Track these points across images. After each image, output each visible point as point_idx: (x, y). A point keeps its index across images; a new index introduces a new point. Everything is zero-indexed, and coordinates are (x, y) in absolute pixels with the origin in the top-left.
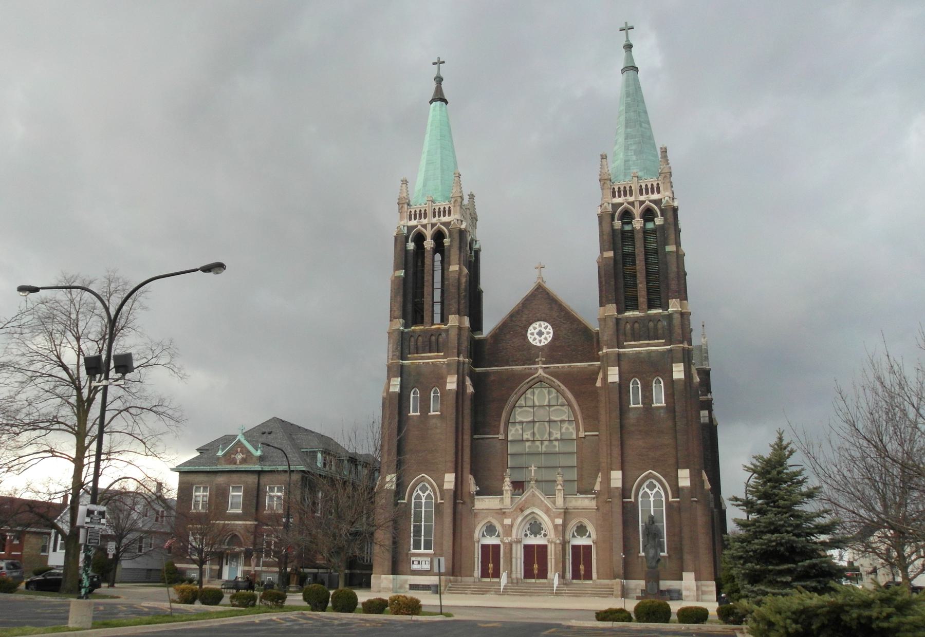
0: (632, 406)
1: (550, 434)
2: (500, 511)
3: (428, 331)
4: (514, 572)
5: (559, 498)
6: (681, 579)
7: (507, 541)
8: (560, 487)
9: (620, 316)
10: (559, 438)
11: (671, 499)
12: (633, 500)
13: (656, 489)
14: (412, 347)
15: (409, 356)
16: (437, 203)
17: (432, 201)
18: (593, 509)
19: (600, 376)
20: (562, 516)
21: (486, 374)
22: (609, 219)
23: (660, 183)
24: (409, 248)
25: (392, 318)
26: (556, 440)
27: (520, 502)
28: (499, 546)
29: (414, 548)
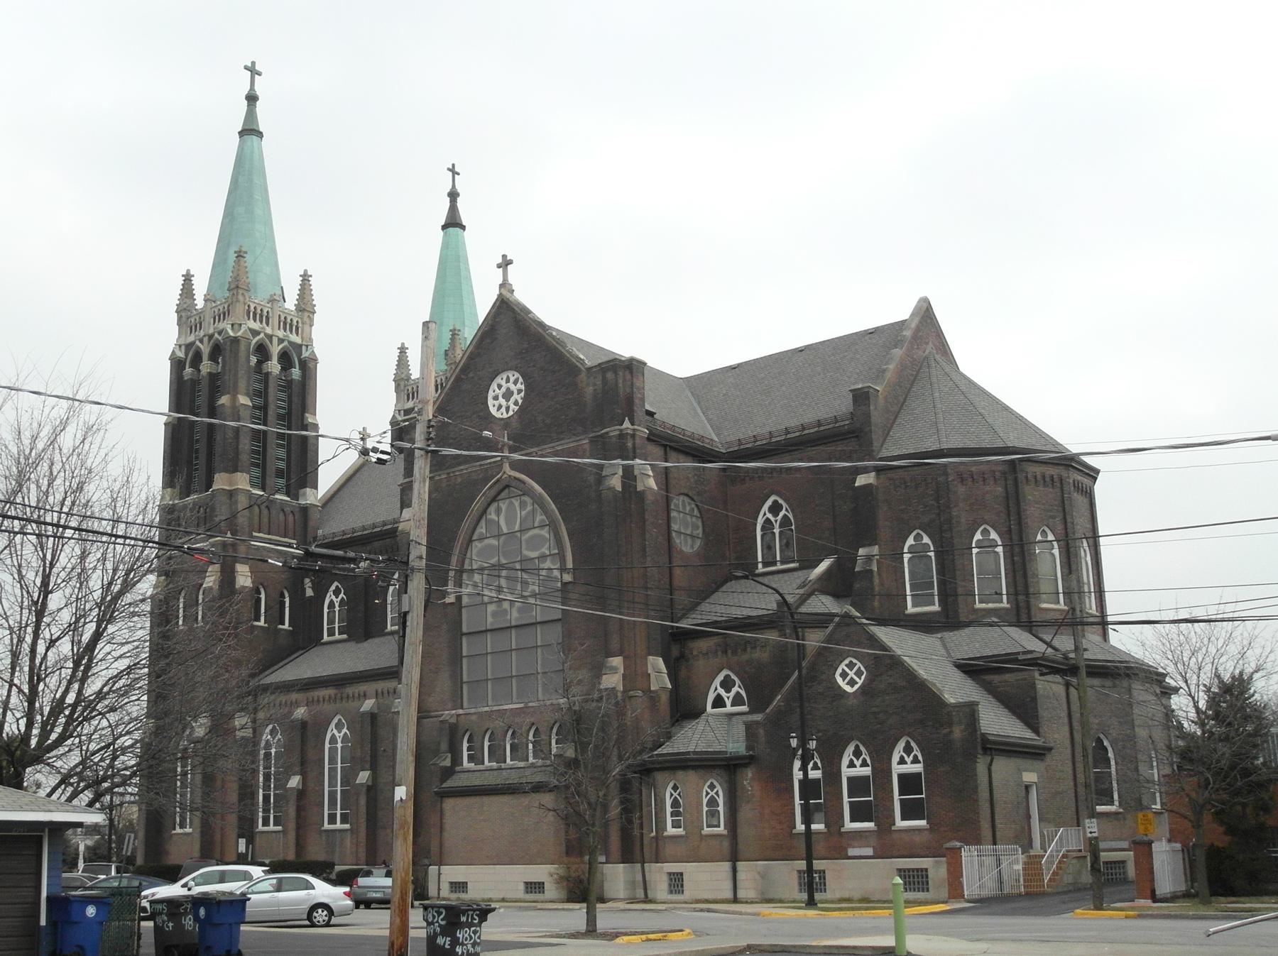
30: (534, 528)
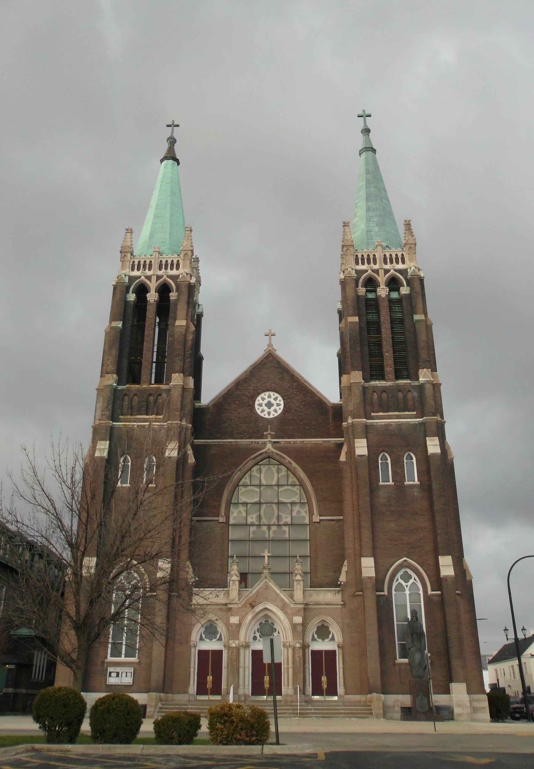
0: (381, 483)
1: (278, 518)
2: (224, 607)
3: (145, 390)
4: (241, 687)
5: (299, 590)
6: (447, 691)
7: (234, 645)
8: (298, 577)
9: (367, 385)
10: (290, 523)
11: (430, 592)
12: (386, 593)
13: (412, 581)
14: (125, 408)
15: (121, 417)
16: (164, 256)
17: (159, 253)
18: (339, 604)
19: (345, 449)
20: (302, 612)
21: (206, 447)
22: (353, 284)
23: (404, 253)
24: (129, 299)
25: (103, 373)
26: (286, 525)
27: (251, 595)
28: (220, 652)
29: (112, 656)
30: (288, 485)
